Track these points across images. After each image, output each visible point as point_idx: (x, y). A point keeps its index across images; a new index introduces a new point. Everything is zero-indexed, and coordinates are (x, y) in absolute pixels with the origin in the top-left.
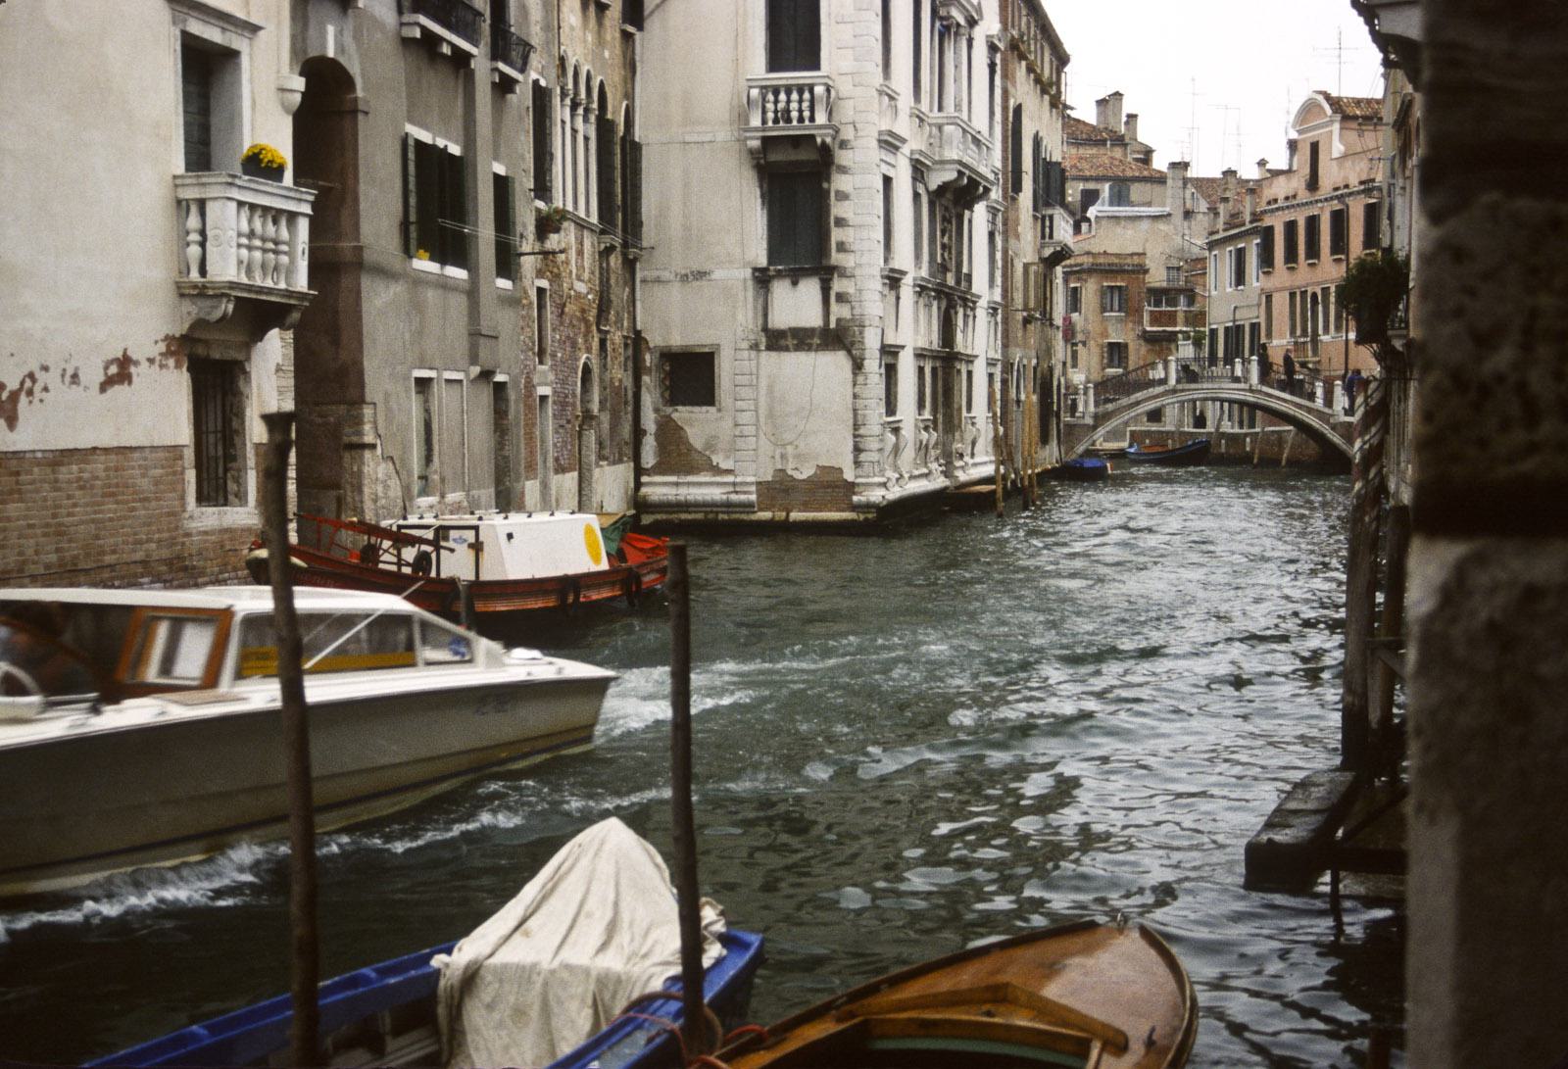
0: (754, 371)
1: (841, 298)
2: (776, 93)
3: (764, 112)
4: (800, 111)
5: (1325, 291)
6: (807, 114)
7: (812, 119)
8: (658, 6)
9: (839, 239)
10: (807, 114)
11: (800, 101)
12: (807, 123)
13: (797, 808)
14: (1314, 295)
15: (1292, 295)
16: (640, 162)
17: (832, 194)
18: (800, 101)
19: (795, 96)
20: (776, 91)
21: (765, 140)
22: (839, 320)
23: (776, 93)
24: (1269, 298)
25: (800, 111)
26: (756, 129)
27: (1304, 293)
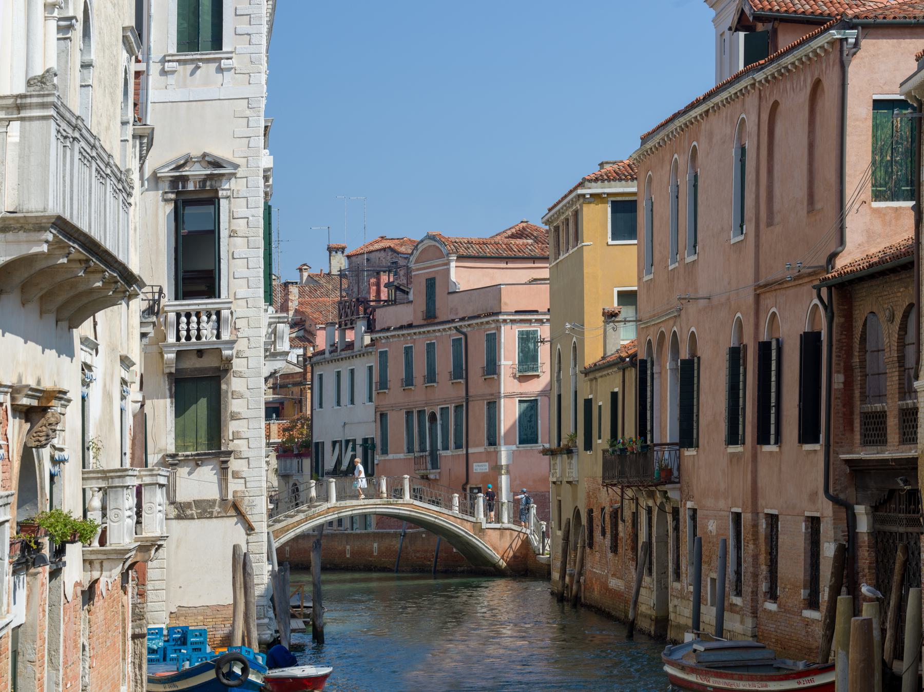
0: (100, 561)
1: (236, 475)
2: (188, 315)
3: (178, 331)
4: (188, 330)
5: (444, 411)
8: (716, 2)
10: (194, 333)
11: (188, 323)
14: (433, 417)
15: (409, 414)
17: (230, 394)
18: (188, 323)
21: (179, 354)
22: (235, 492)
23: (188, 315)
24: (383, 416)
25: (188, 330)
26: (173, 345)
27: (421, 413)
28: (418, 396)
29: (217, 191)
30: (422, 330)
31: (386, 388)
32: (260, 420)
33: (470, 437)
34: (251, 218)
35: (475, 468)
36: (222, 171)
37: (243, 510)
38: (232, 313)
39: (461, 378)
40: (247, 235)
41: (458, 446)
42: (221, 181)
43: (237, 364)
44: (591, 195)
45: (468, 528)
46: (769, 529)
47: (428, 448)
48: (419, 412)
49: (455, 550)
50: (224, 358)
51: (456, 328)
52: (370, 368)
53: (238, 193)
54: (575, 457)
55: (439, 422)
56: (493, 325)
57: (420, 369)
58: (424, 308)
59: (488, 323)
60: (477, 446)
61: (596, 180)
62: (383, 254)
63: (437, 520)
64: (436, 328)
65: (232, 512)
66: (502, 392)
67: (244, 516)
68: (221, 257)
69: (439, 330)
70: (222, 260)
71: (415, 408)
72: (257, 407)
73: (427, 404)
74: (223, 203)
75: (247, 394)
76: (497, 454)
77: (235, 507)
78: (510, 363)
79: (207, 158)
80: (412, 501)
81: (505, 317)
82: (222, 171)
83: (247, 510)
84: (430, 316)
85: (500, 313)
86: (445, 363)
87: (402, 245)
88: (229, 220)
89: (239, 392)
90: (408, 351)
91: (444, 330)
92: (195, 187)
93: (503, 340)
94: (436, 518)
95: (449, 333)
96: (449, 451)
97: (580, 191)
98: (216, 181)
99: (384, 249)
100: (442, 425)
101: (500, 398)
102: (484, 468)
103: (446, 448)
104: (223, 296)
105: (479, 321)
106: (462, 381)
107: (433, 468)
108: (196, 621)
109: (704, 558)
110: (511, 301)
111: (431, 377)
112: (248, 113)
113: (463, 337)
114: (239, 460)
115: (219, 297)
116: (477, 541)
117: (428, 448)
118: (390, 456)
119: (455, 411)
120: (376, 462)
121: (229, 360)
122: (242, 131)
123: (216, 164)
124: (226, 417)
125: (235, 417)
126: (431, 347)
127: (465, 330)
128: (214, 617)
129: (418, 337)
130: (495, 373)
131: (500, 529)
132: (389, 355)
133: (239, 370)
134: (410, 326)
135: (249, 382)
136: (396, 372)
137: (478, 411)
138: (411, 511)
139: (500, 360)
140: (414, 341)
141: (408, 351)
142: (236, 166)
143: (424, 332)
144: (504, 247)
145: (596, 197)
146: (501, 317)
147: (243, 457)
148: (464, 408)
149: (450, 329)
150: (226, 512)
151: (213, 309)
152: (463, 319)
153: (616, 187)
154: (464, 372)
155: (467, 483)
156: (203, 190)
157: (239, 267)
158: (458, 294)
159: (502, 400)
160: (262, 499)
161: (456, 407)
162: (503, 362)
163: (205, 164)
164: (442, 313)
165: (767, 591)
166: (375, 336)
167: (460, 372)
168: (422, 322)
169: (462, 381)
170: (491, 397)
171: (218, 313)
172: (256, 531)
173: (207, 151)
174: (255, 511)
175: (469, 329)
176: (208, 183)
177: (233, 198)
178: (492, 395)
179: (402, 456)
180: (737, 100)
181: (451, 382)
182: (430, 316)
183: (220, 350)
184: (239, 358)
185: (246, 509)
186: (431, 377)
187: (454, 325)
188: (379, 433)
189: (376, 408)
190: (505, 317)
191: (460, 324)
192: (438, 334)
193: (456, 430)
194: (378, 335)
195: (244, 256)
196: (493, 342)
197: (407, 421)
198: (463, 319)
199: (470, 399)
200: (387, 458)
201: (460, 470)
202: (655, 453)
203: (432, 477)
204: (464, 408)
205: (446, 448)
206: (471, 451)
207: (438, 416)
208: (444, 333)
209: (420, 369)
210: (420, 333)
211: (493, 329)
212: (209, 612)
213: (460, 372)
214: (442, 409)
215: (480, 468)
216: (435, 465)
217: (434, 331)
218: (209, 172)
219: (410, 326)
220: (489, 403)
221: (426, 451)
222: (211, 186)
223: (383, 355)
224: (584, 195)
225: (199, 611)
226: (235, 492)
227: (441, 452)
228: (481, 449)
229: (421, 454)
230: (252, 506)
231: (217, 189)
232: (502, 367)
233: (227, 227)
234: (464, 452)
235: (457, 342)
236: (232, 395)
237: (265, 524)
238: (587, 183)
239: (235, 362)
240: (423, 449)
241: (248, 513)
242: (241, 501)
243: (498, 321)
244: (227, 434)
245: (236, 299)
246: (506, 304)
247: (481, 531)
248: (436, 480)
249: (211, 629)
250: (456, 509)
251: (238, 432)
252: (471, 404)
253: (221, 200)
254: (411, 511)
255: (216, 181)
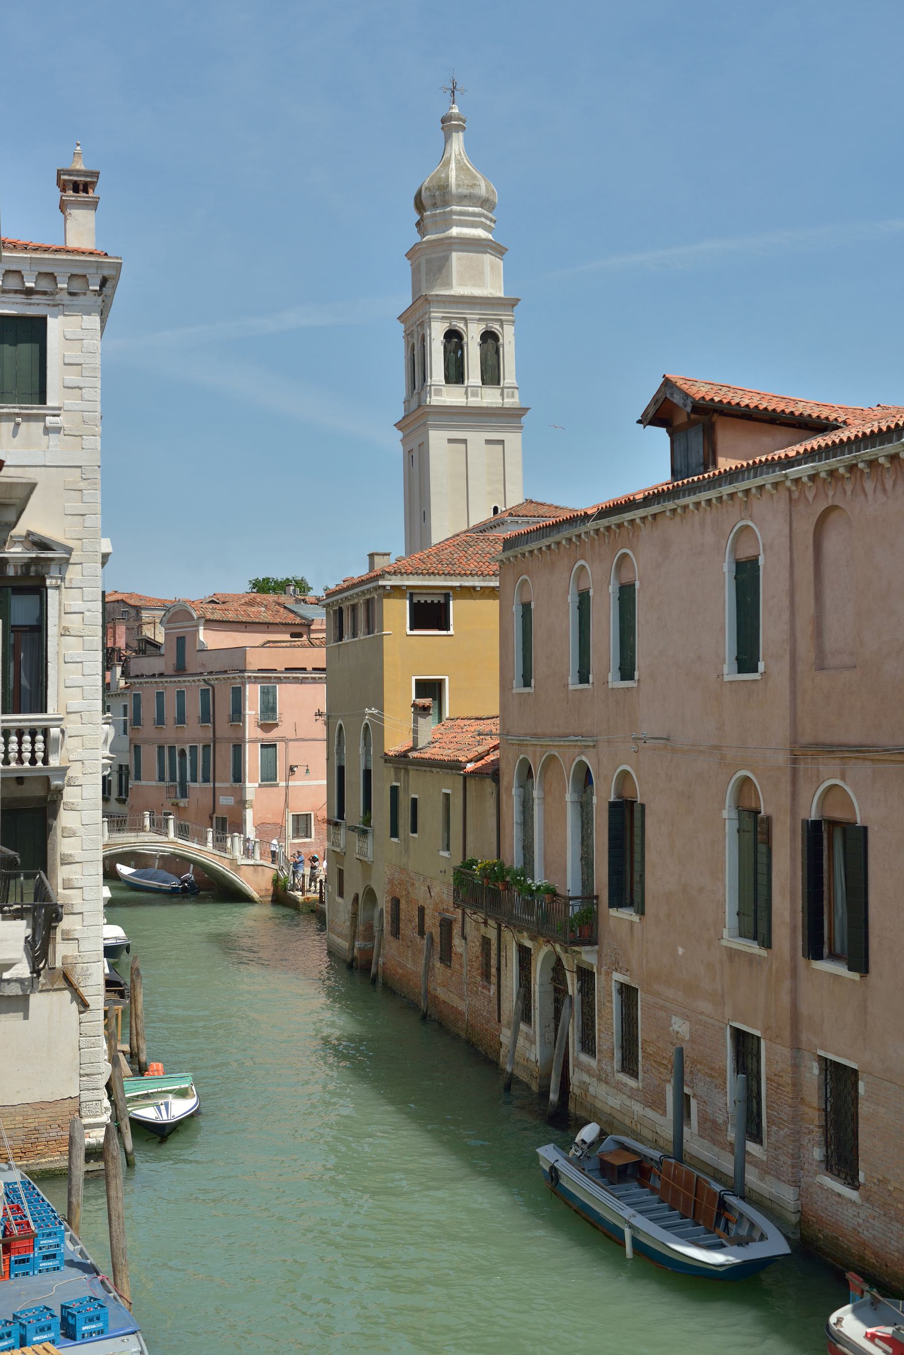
4: (33, 752)
5: (193, 749)
6: (40, 755)
7: (45, 761)
9: (65, 877)
10: (40, 755)
12: (40, 764)
13: (475, 1161)
14: (183, 753)
15: (161, 748)
16: (764, 1215)
19: (27, 738)
20: (20, 733)
22: (65, 958)
24: (137, 748)
27: (172, 748)
28: (170, 732)
29: (44, 579)
30: (173, 679)
31: (140, 725)
32: (97, 864)
33: (217, 773)
34: (87, 613)
35: (221, 800)
36: (50, 555)
37: (74, 981)
38: (63, 732)
39: (209, 722)
40: (81, 634)
41: (206, 780)
42: (49, 566)
43: (69, 795)
44: (392, 586)
45: (226, 864)
46: (823, 1076)
47: (178, 779)
48: (170, 747)
49: (206, 876)
50: (52, 788)
51: (204, 680)
52: (125, 707)
53: (71, 582)
54: (370, 837)
55: (188, 757)
56: (239, 680)
57: (171, 712)
58: (174, 661)
59: (234, 678)
60: (223, 782)
61: (395, 573)
62: (116, 605)
63: (198, 857)
64: (186, 679)
65: (62, 984)
66: (247, 737)
67: (76, 990)
68: (49, 660)
69: (189, 681)
70: (49, 664)
71: (166, 744)
72: (93, 848)
73: (177, 742)
74: (52, 594)
75: (81, 830)
76: (242, 790)
77: (66, 978)
78: (254, 713)
79: (30, 538)
80: (176, 839)
81: (250, 674)
82: (50, 555)
83: (80, 981)
84: (180, 669)
85: (244, 671)
86: (194, 708)
87: (131, 599)
88: (60, 614)
89: (70, 829)
90: (160, 695)
91: (194, 681)
92: (16, 572)
93: (247, 694)
94: (197, 855)
95: (197, 684)
96: (197, 784)
97: (381, 583)
98: (42, 566)
99: (118, 601)
100: (191, 760)
101: (245, 742)
102: (230, 801)
103: (194, 780)
104: (50, 710)
105: (226, 676)
106: (210, 725)
107: (182, 797)
108: (14, 1122)
109: (687, 1077)
110: (256, 660)
111: (181, 719)
112: (82, 485)
113: (210, 688)
114: (71, 916)
115: (46, 712)
116: (232, 875)
117: (178, 779)
118: (143, 783)
119: (203, 749)
120: (130, 786)
121: (59, 791)
122: (75, 506)
123: (43, 545)
124: (55, 860)
125: (67, 861)
126: (181, 694)
127: (212, 682)
128: (37, 1116)
129: (168, 685)
130: (240, 721)
131: (253, 865)
132: (142, 697)
133: (70, 801)
134: (161, 675)
135: (83, 817)
136: (149, 712)
137: (224, 753)
138: (175, 849)
139: (245, 710)
140: (166, 688)
141: (160, 695)
142: (69, 550)
143: (175, 681)
144: (243, 613)
145: (397, 591)
146: (246, 674)
147: (76, 911)
148: (212, 748)
149: (199, 680)
150: (53, 984)
151: (40, 727)
152: (211, 673)
153: (414, 580)
154: (211, 718)
155: (214, 812)
156: (26, 575)
157: (73, 675)
158: (206, 652)
159: (247, 745)
160: (98, 966)
161: (204, 747)
162: (247, 712)
163: (29, 545)
164: (191, 667)
165: (822, 1159)
166: (129, 681)
167: (207, 716)
168: (173, 673)
169: (210, 725)
170: (236, 741)
171: (45, 732)
172: (91, 1008)
173: (32, 529)
174: (90, 982)
175: (216, 682)
176: (33, 569)
177: (66, 588)
178: (238, 739)
179: (153, 783)
180: (730, 502)
181: (199, 725)
182: (180, 669)
183: (47, 779)
184: (71, 786)
185: (78, 979)
186: (181, 719)
187: (203, 678)
188: (133, 762)
189: (130, 740)
190: (250, 674)
191: (209, 677)
192: (187, 684)
193: (204, 765)
194: (132, 680)
195: (78, 660)
196: (238, 696)
197: (159, 754)
198: (211, 673)
199: (217, 741)
200: (140, 784)
201: (208, 800)
202: (571, 907)
203: (182, 805)
204: (212, 748)
205: (194, 780)
206: (217, 785)
207: (188, 753)
208: (193, 684)
209: (171, 712)
210: (171, 682)
211: (239, 683)
212: (30, 1111)
213: (207, 716)
214: (191, 746)
215: (225, 801)
216: (184, 795)
217: (184, 681)
218: (34, 555)
219: (161, 675)
220: (234, 746)
221: (176, 781)
222: (36, 571)
223: (137, 697)
224: (384, 587)
225: (17, 1110)
226: (65, 958)
227: (190, 784)
228: (227, 785)
229: (172, 783)
230: (87, 976)
231: (44, 576)
232: (247, 716)
233: (57, 623)
234: (212, 785)
235: (205, 693)
236: (63, 832)
237: (101, 999)
238: (387, 575)
239: (67, 791)
240: (173, 779)
241: (82, 985)
242: (72, 970)
243: (243, 677)
244: (55, 883)
245: (68, 713)
246: (250, 663)
247: (237, 868)
248: (185, 808)
249: (34, 1132)
250: (210, 845)
251: (69, 880)
252: (217, 746)
253: (49, 591)
254: (175, 849)
255: (42, 566)
